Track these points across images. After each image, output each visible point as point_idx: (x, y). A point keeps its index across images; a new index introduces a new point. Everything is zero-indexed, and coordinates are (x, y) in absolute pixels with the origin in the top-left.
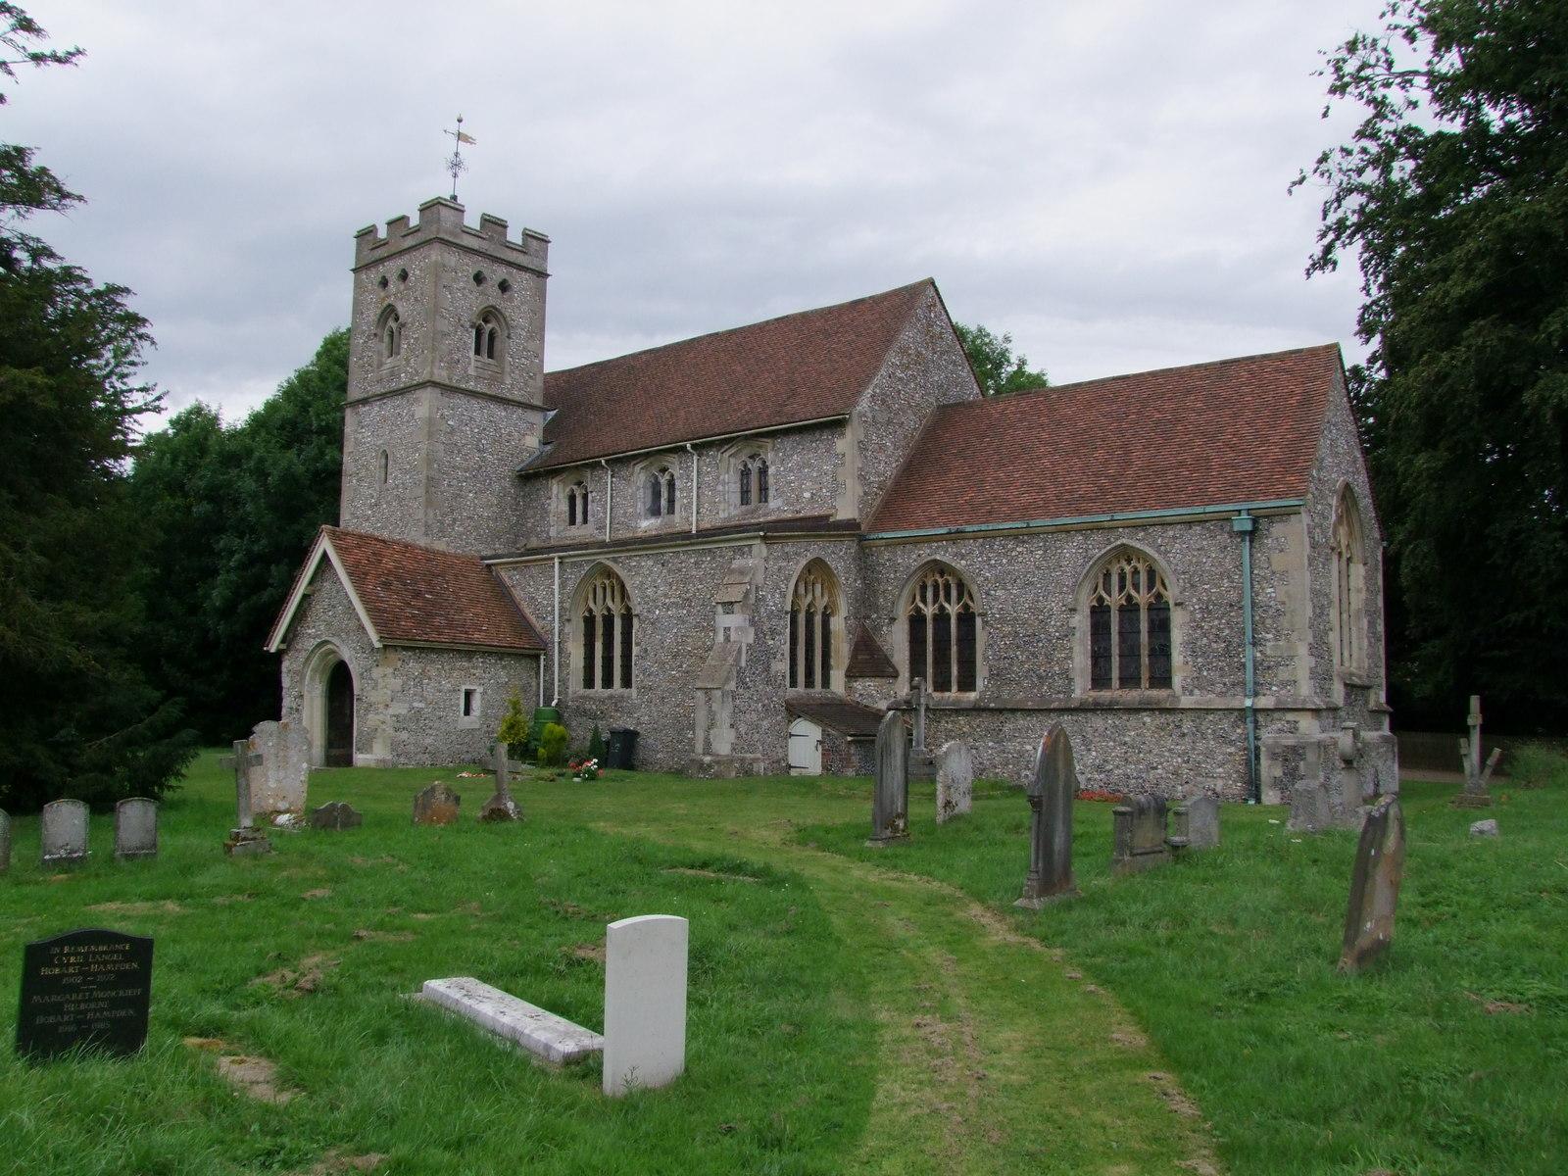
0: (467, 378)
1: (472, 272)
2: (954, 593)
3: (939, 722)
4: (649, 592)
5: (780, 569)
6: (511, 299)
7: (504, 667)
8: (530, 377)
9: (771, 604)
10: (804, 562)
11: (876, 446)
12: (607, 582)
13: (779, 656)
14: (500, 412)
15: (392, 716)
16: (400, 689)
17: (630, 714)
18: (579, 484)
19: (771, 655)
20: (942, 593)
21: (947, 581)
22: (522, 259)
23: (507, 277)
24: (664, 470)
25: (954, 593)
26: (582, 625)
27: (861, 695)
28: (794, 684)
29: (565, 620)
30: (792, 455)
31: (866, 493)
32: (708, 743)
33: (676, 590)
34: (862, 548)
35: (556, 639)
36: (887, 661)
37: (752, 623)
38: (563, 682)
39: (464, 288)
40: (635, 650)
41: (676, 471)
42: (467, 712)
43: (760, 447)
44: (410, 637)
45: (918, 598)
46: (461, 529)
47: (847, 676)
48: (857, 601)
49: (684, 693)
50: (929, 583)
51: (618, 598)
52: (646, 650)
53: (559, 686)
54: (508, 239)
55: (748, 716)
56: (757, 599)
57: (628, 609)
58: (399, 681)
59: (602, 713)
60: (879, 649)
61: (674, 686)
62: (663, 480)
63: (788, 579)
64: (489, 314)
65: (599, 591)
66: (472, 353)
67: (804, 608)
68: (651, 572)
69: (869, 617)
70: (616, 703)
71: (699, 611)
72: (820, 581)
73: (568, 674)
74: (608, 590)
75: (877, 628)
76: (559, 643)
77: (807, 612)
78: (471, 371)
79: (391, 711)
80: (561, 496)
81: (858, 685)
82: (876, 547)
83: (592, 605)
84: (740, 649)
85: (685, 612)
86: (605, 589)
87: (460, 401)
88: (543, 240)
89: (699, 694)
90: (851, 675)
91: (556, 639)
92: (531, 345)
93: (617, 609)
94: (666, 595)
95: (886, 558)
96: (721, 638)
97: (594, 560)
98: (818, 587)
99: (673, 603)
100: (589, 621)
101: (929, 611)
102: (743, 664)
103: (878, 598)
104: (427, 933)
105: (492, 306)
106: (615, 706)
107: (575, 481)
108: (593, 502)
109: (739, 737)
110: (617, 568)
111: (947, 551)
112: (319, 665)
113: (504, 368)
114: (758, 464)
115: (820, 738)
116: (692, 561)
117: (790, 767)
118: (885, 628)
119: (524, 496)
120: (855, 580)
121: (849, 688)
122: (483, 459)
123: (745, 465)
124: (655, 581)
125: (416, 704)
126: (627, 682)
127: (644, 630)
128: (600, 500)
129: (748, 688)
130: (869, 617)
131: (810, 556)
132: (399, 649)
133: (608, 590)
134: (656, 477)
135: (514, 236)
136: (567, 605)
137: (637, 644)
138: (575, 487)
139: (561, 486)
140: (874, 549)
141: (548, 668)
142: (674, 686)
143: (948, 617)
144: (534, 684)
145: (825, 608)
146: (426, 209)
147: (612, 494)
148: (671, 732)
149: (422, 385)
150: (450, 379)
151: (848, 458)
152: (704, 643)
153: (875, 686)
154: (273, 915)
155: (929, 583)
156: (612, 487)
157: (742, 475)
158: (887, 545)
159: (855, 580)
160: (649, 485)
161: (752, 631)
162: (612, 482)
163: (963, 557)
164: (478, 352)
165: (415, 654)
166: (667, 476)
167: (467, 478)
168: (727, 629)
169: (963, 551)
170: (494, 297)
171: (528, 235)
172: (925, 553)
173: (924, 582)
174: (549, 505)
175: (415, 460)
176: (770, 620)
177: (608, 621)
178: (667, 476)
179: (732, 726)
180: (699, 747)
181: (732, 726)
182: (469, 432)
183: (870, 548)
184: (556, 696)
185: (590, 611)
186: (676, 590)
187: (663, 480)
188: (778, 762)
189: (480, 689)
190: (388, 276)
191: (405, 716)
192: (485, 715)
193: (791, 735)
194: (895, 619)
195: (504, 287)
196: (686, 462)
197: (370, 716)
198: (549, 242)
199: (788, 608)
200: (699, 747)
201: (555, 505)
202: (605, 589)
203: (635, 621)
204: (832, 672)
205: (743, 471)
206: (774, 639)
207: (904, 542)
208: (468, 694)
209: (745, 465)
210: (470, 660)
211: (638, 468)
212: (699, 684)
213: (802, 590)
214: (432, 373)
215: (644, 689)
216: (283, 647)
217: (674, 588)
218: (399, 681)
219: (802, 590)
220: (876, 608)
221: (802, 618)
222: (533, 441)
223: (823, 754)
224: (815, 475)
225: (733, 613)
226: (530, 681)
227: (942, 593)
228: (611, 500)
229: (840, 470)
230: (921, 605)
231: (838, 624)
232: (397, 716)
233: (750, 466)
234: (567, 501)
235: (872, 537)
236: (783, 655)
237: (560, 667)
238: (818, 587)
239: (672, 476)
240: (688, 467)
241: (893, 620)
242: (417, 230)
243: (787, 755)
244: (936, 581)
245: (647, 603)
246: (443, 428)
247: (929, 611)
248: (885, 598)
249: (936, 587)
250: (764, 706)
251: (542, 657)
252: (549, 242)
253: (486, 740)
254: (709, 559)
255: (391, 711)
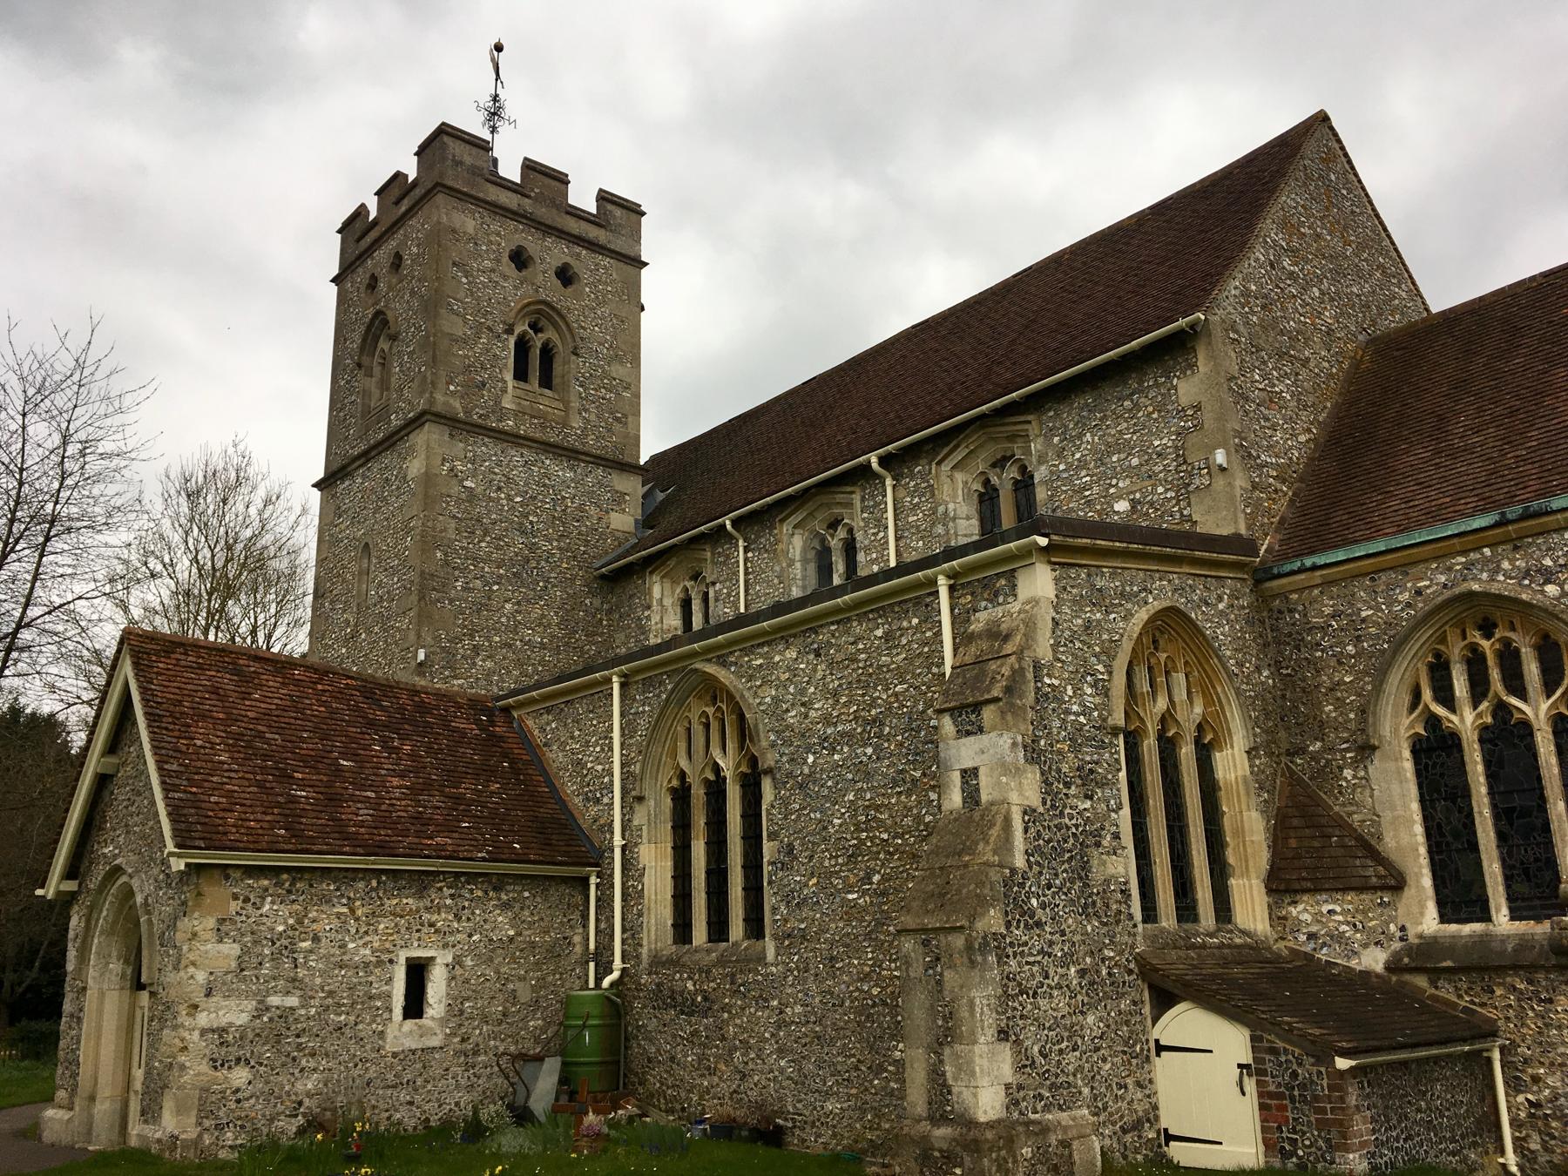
0: (502, 414)
1: (506, 247)
2: (1532, 670)
3: (1551, 1001)
4: (792, 718)
5: (1088, 626)
6: (579, 296)
7: (506, 906)
8: (617, 419)
9: (1075, 708)
10: (1142, 616)
11: (1263, 395)
12: (710, 710)
13: (1107, 841)
14: (561, 472)
15: (203, 1032)
16: (234, 964)
17: (762, 1000)
18: (695, 577)
19: (1093, 835)
20: (1495, 675)
21: (1507, 643)
22: (593, 233)
23: (568, 260)
24: (833, 525)
25: (1532, 670)
26: (668, 802)
27: (1312, 936)
28: (1150, 913)
29: (633, 800)
30: (1080, 436)
31: (1255, 486)
32: (939, 1087)
33: (847, 705)
34: (1263, 600)
35: (618, 841)
36: (1369, 849)
37: (1033, 754)
38: (632, 930)
39: (493, 271)
40: (768, 849)
41: (857, 519)
42: (415, 1006)
43: (1012, 438)
44: (264, 845)
45: (1427, 695)
46: (489, 664)
47: (1270, 891)
48: (1267, 715)
49: (878, 946)
50: (1456, 651)
51: (731, 745)
52: (791, 848)
53: (623, 942)
54: (570, 201)
55: (1042, 1002)
56: (1041, 697)
57: (753, 761)
58: (231, 949)
59: (705, 999)
60: (1342, 824)
61: (854, 928)
62: (835, 543)
63: (1109, 653)
64: (541, 315)
65: (698, 729)
66: (509, 376)
67: (1152, 728)
68: (794, 672)
69: (1301, 751)
70: (733, 975)
71: (901, 744)
72: (1180, 664)
73: (640, 914)
74: (714, 726)
75: (1327, 773)
76: (624, 848)
77: (1161, 736)
78: (508, 403)
79: (203, 1019)
80: (668, 602)
81: (1302, 911)
82: (1300, 590)
83: (684, 763)
84: (1007, 821)
85: (869, 751)
86: (707, 726)
87: (486, 448)
88: (635, 211)
89: (908, 945)
90: (1281, 886)
91: (618, 841)
92: (618, 370)
93: (728, 764)
94: (827, 720)
95: (1328, 611)
96: (955, 799)
97: (685, 668)
98: (1179, 678)
99: (843, 734)
100: (681, 796)
101: (1467, 721)
102: (1020, 862)
103: (1319, 706)
104: (839, 1059)
105: (544, 302)
106: (732, 983)
107: (691, 573)
108: (717, 600)
109: (1024, 1064)
110: (723, 675)
111: (1498, 570)
112: (115, 922)
113: (569, 402)
114: (1012, 473)
115: (1246, 1057)
116: (879, 633)
117: (1170, 1138)
118: (1348, 773)
119: (610, 612)
120: (1258, 669)
121: (1278, 920)
122: (533, 548)
123: (987, 482)
124: (803, 692)
125: (274, 1000)
126: (755, 926)
127: (785, 803)
128: (729, 595)
129: (1039, 924)
130: (1301, 751)
131: (1155, 605)
132: (237, 874)
133: (714, 726)
134: (823, 540)
135: (582, 197)
136: (636, 768)
137: (773, 836)
138: (689, 584)
139: (667, 585)
140: (1295, 596)
141: (605, 903)
142: (854, 928)
143: (1526, 728)
144: (577, 939)
145: (1200, 728)
146: (424, 151)
147: (746, 582)
148: (853, 1043)
149: (414, 424)
150: (467, 412)
151: (1208, 418)
152: (918, 819)
153: (1344, 912)
154: (815, 1023)
155: (1456, 651)
156: (746, 569)
157: (981, 502)
158: (1328, 583)
159: (1258, 669)
160: (811, 555)
161: (1032, 777)
162: (746, 560)
163: (1548, 576)
164: (521, 374)
165: (279, 884)
166: (842, 533)
167: (500, 576)
168: (970, 774)
169: (1548, 562)
170: (551, 290)
171: (604, 197)
172: (1435, 581)
173: (1438, 655)
174: (648, 618)
175: (406, 548)
176: (1076, 748)
177: (716, 791)
178: (842, 533)
179: (1003, 1034)
180: (917, 1098)
181: (1003, 1034)
182: (505, 502)
183: (1284, 596)
184: (618, 963)
185: (682, 775)
186: (847, 705)
187: (835, 543)
188: (1137, 1126)
189: (444, 958)
190: (377, 272)
191: (242, 1029)
192: (455, 1010)
193: (1160, 1048)
194: (1374, 748)
195: (565, 276)
196: (873, 497)
197: (165, 1032)
198: (643, 214)
199: (1118, 718)
200: (917, 1098)
201: (658, 618)
202: (707, 726)
203: (767, 786)
204: (1232, 882)
205: (981, 495)
206: (1089, 797)
207: (1372, 570)
208: (417, 973)
209: (987, 482)
210: (420, 894)
211: (786, 528)
212: (909, 921)
213: (1144, 686)
214: (432, 401)
215: (787, 938)
216: (71, 886)
217: (843, 699)
218: (231, 949)
219: (1144, 686)
220: (1320, 728)
221: (1150, 747)
222: (623, 521)
223: (1262, 1107)
224: (1135, 462)
225: (981, 730)
226: (568, 933)
227: (1495, 675)
228: (746, 591)
229: (1193, 439)
230: (1439, 710)
231: (1232, 764)
232: (222, 1031)
233: (995, 480)
234: (679, 610)
235: (1287, 568)
236: (1116, 836)
237: (624, 900)
238: (1179, 678)
239: (851, 531)
240: (877, 505)
241: (1366, 750)
242: (415, 183)
243: (1155, 1107)
244: (1474, 648)
245: (787, 743)
246: (455, 490)
247: (1467, 721)
248: (1340, 703)
249: (1476, 664)
250: (1082, 973)
251: (593, 880)
252: (643, 214)
253: (459, 1070)
254: (915, 621)
255: (203, 1019)
